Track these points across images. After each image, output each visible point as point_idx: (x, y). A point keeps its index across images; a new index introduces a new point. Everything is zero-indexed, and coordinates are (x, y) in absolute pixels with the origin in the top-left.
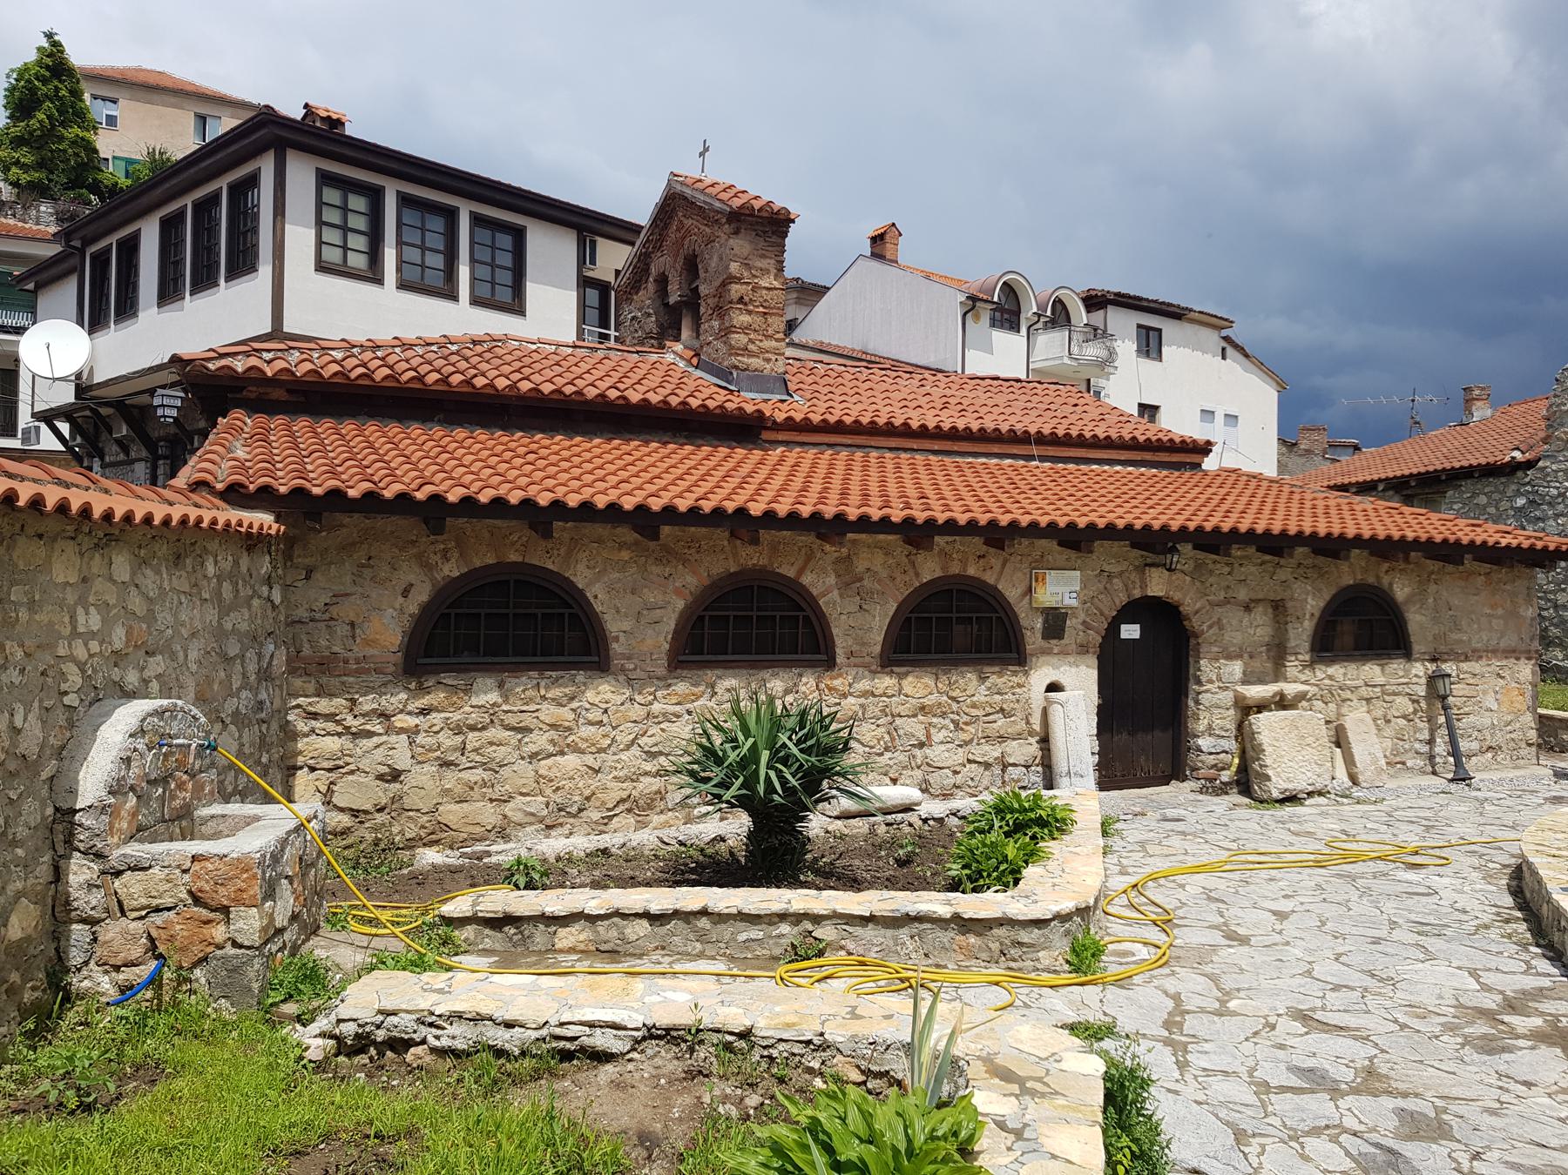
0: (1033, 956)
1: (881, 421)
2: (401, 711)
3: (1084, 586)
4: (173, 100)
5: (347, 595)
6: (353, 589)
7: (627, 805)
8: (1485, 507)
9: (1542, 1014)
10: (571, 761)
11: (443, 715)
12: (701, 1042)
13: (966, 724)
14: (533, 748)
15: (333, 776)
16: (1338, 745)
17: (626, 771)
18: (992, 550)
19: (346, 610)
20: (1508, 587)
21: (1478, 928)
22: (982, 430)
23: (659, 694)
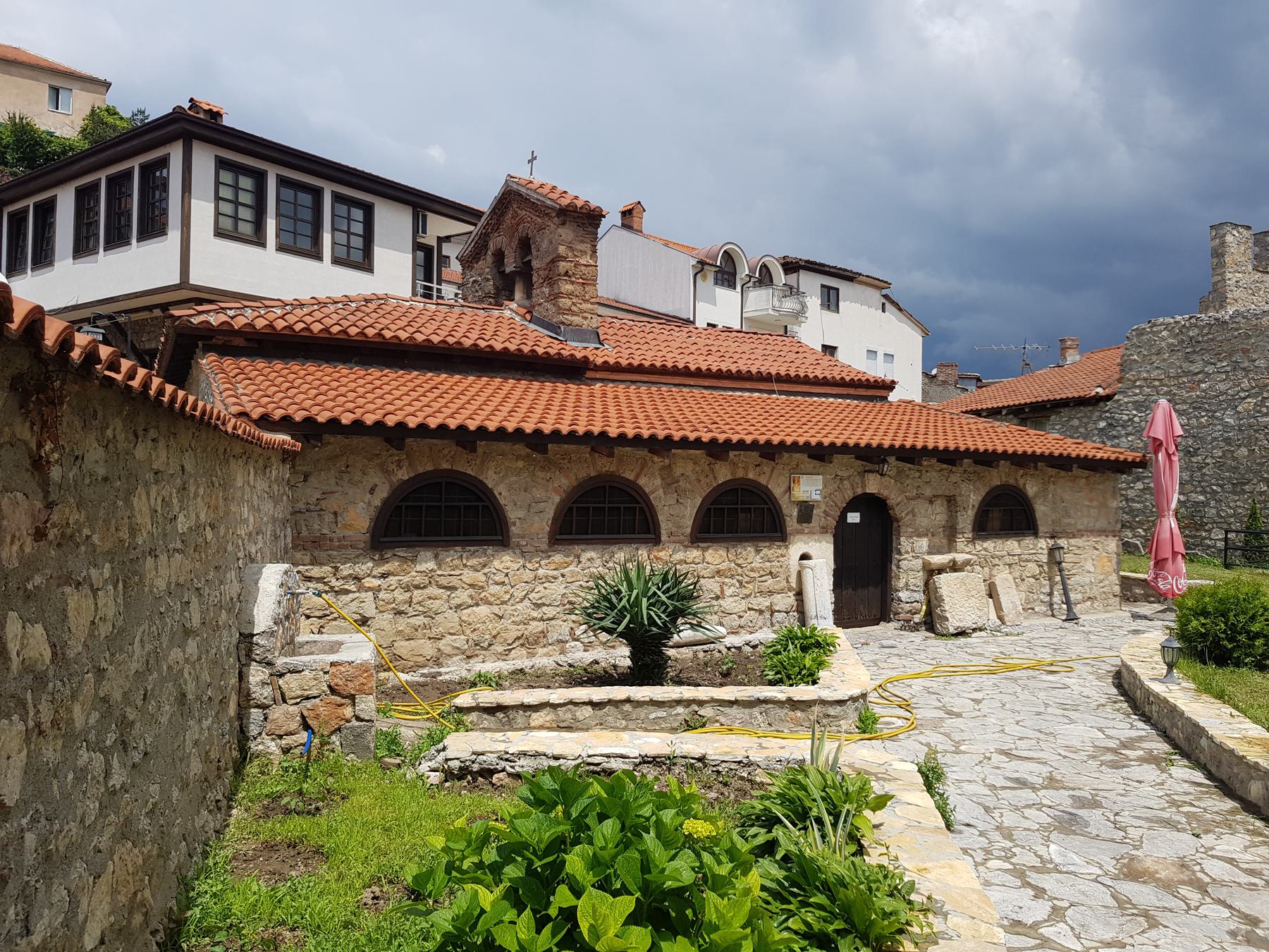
0: (837, 723)
1: (669, 365)
2: (369, 575)
3: (825, 486)
4: (30, 73)
5: (332, 492)
6: (337, 489)
7: (521, 641)
8: (1077, 428)
9: (1143, 749)
10: (483, 610)
11: (397, 578)
12: (675, 764)
13: (747, 583)
14: (458, 601)
15: (322, 621)
16: (991, 597)
17: (520, 617)
18: (765, 461)
19: (332, 503)
20: (1100, 487)
21: (1098, 706)
22: (739, 371)
23: (543, 562)
